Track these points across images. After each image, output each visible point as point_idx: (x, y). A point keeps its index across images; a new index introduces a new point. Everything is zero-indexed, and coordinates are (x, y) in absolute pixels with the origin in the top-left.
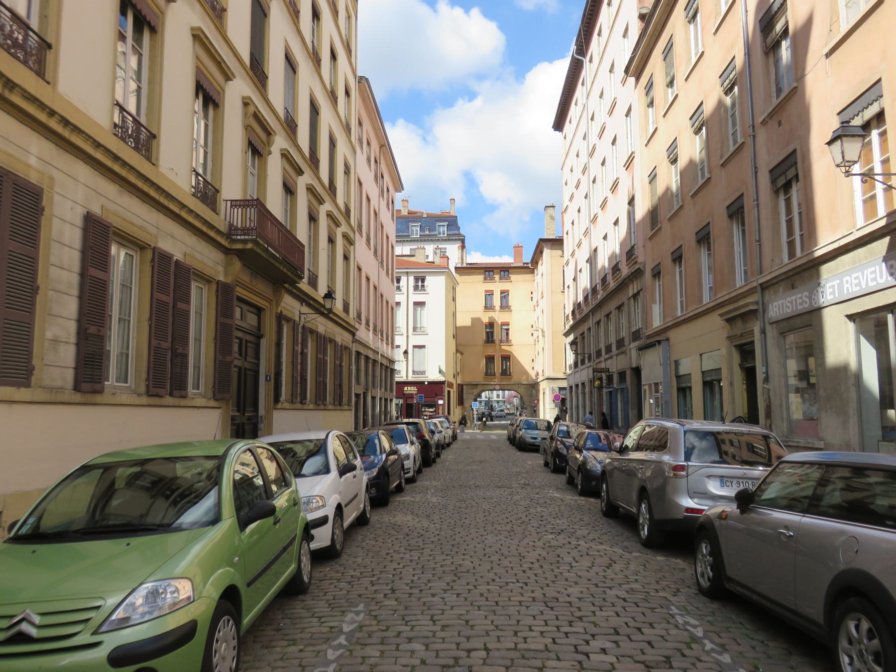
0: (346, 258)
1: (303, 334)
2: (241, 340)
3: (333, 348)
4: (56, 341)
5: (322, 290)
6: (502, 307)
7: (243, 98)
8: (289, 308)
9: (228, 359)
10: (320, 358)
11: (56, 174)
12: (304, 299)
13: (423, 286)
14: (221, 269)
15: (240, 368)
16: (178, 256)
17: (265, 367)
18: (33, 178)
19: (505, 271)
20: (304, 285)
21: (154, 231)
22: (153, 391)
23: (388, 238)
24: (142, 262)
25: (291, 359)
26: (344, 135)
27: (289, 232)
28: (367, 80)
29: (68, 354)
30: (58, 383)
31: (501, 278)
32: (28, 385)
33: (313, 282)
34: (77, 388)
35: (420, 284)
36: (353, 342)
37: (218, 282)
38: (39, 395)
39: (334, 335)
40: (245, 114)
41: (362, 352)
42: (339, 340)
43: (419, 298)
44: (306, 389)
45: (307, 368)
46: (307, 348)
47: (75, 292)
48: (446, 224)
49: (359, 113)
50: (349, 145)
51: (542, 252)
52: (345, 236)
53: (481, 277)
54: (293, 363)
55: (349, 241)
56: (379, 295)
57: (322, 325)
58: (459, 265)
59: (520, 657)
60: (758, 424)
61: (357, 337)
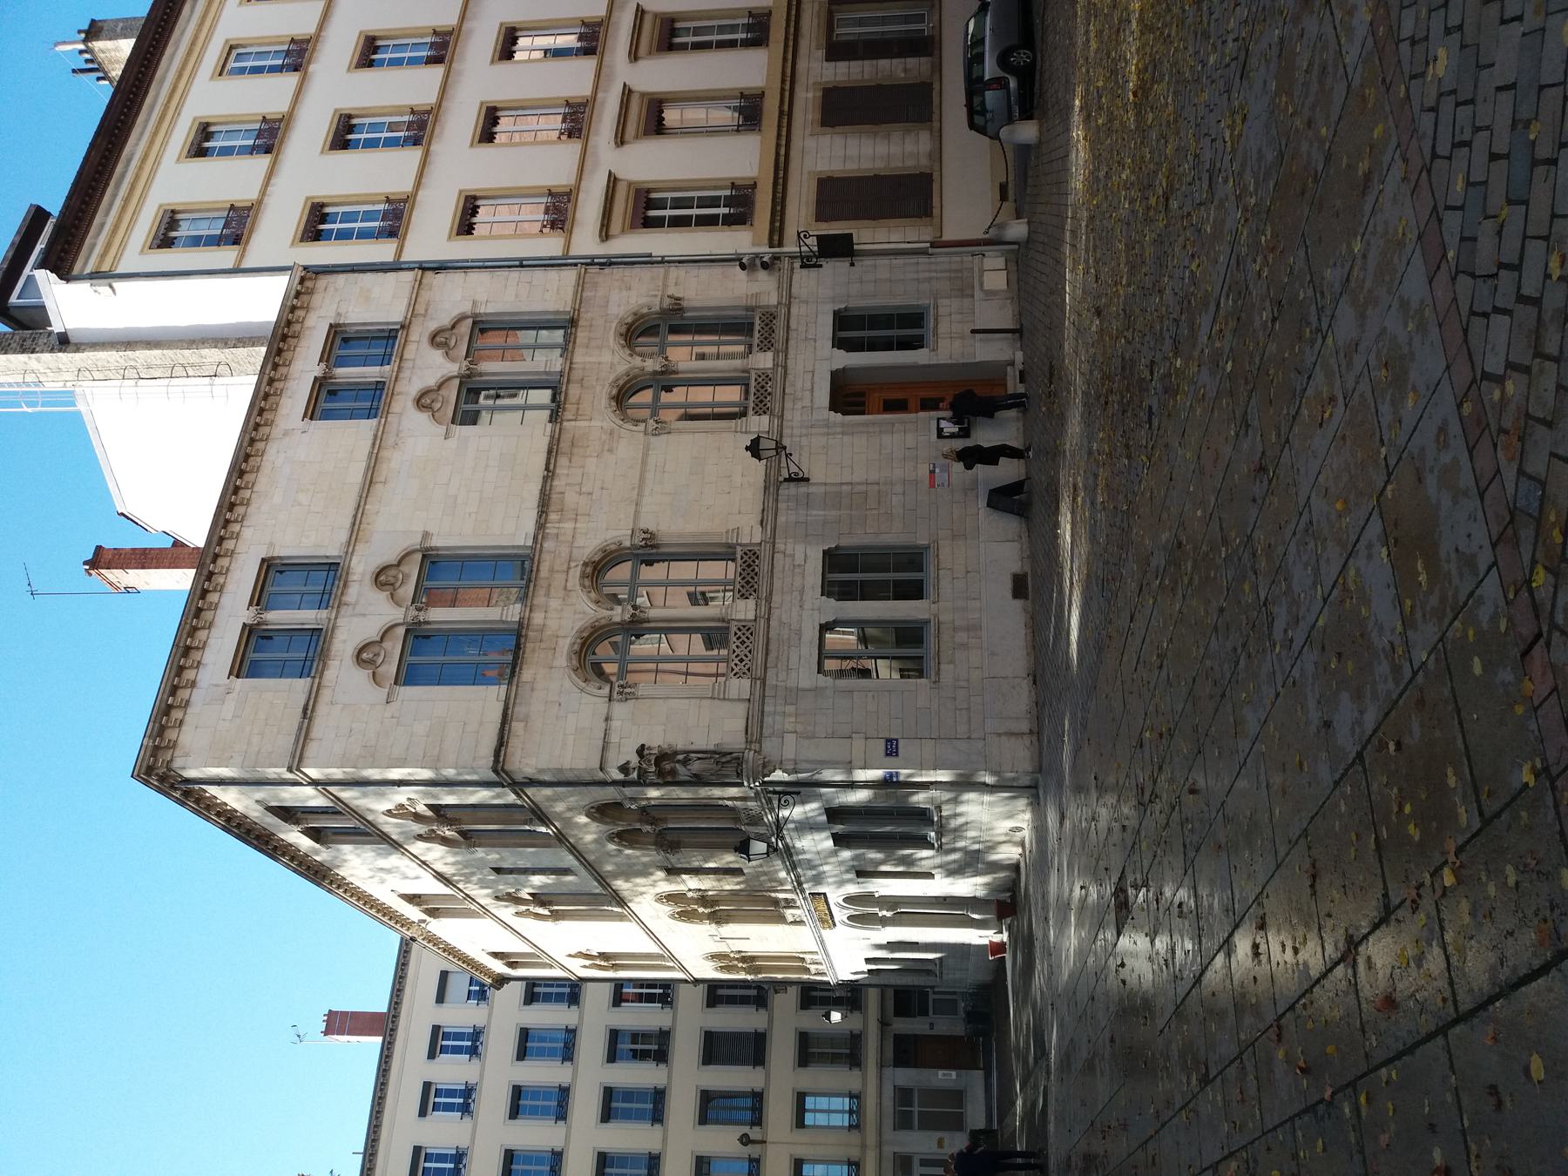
4: (905, 70)
18: (820, 94)
29: (912, 62)
34: (931, 55)
47: (875, 62)
59: (1028, 731)
60: (895, 1035)
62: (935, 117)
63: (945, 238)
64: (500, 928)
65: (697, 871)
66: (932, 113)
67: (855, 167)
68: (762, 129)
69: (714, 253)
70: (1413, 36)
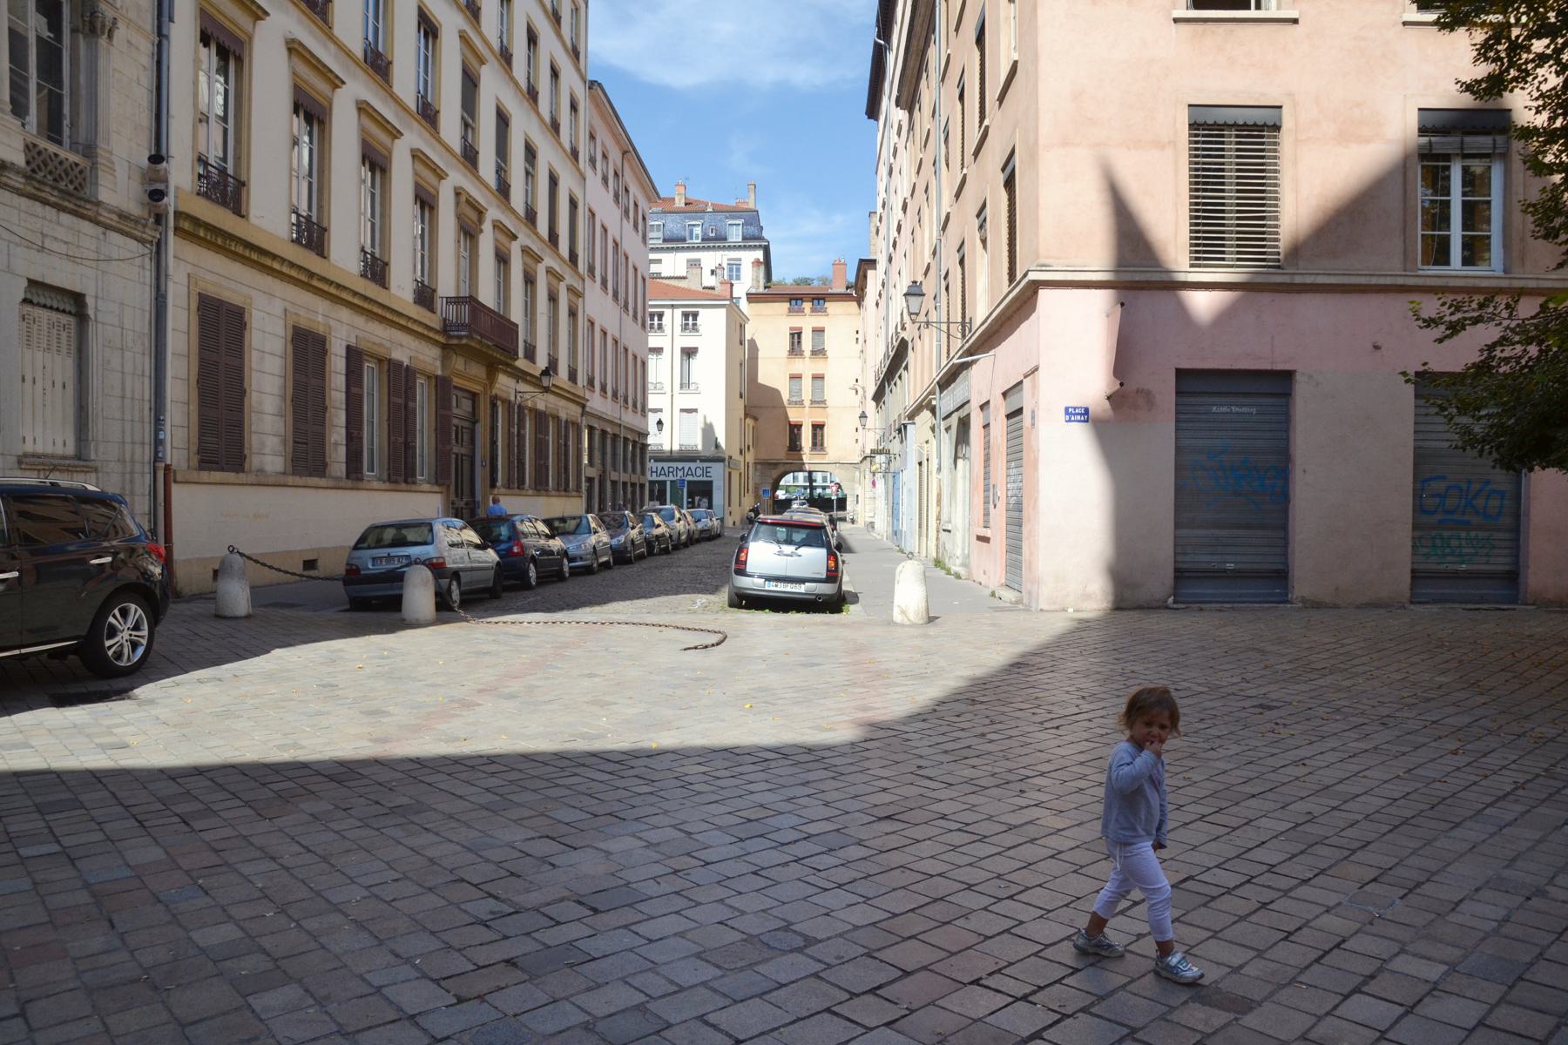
0: (573, 314)
1: (519, 413)
2: (457, 427)
3: (556, 425)
4: (336, 444)
5: (542, 362)
6: (814, 353)
7: (455, 188)
8: (504, 388)
9: (448, 447)
10: (540, 439)
11: (332, 322)
12: (521, 376)
13: (695, 325)
14: (438, 363)
15: (457, 455)
16: (406, 362)
17: (481, 451)
18: (321, 330)
19: (819, 299)
20: (521, 363)
21: (388, 344)
22: (393, 478)
23: (636, 270)
24: (380, 372)
25: (506, 441)
26: (569, 163)
27: (502, 317)
28: (600, 85)
30: (339, 474)
31: (813, 310)
32: (324, 477)
33: (530, 354)
34: (348, 477)
35: (691, 322)
36: (582, 416)
37: (437, 377)
38: (252, 478)
39: (558, 410)
40: (457, 204)
41: (596, 425)
42: (563, 416)
43: (689, 341)
44: (524, 473)
45: (525, 451)
46: (524, 428)
48: (741, 222)
49: (591, 126)
50: (577, 173)
51: (865, 277)
52: (570, 289)
53: (787, 305)
54: (509, 445)
55: (575, 293)
56: (621, 349)
57: (542, 402)
58: (753, 291)
61: (587, 409)
62: (298, 480)
63: (175, 488)
64: (615, 106)
65: (70, 202)
66: (301, 475)
67: (254, 366)
68: (199, 197)
69: (171, 121)
70: (669, 1026)
